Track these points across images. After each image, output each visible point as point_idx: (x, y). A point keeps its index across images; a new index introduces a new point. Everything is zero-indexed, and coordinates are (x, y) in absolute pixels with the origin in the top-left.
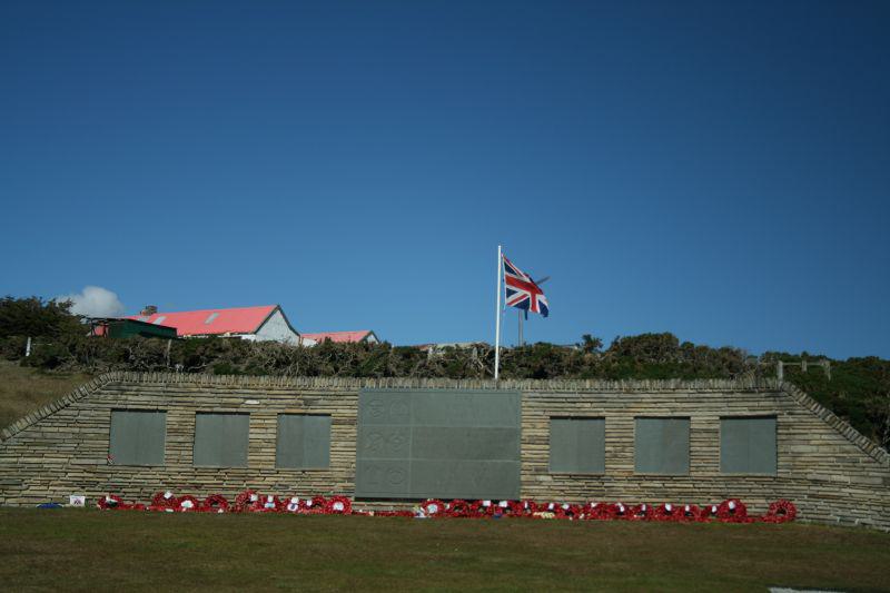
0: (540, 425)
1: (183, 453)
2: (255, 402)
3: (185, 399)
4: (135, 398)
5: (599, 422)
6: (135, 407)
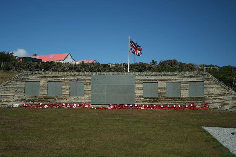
1: (45, 93)
2: (64, 79)
4: (31, 78)
5: (156, 83)
6: (31, 80)
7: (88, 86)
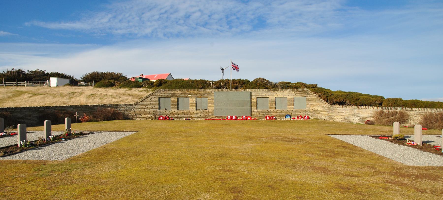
0: (254, 99)
1: (175, 107)
2: (190, 95)
3: (175, 95)
4: (164, 95)
6: (164, 97)
7: (211, 101)
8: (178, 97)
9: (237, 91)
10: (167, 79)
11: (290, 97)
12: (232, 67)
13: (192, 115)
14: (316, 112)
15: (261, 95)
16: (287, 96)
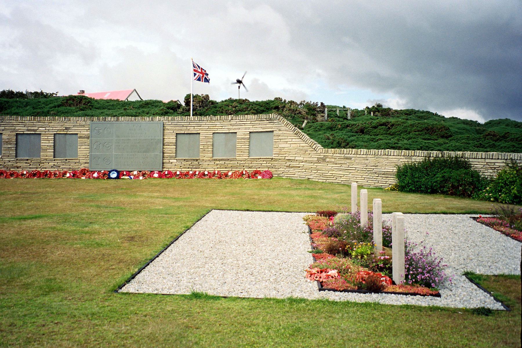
2: (43, 129)
7: (85, 140)
8: (17, 132)
9: (137, 120)
10: (129, 99)
11: (242, 132)
12: (195, 74)
13: (46, 168)
14: (293, 164)
15: (186, 128)
16: (235, 131)
